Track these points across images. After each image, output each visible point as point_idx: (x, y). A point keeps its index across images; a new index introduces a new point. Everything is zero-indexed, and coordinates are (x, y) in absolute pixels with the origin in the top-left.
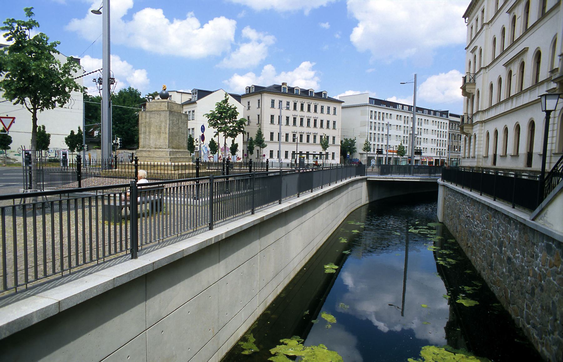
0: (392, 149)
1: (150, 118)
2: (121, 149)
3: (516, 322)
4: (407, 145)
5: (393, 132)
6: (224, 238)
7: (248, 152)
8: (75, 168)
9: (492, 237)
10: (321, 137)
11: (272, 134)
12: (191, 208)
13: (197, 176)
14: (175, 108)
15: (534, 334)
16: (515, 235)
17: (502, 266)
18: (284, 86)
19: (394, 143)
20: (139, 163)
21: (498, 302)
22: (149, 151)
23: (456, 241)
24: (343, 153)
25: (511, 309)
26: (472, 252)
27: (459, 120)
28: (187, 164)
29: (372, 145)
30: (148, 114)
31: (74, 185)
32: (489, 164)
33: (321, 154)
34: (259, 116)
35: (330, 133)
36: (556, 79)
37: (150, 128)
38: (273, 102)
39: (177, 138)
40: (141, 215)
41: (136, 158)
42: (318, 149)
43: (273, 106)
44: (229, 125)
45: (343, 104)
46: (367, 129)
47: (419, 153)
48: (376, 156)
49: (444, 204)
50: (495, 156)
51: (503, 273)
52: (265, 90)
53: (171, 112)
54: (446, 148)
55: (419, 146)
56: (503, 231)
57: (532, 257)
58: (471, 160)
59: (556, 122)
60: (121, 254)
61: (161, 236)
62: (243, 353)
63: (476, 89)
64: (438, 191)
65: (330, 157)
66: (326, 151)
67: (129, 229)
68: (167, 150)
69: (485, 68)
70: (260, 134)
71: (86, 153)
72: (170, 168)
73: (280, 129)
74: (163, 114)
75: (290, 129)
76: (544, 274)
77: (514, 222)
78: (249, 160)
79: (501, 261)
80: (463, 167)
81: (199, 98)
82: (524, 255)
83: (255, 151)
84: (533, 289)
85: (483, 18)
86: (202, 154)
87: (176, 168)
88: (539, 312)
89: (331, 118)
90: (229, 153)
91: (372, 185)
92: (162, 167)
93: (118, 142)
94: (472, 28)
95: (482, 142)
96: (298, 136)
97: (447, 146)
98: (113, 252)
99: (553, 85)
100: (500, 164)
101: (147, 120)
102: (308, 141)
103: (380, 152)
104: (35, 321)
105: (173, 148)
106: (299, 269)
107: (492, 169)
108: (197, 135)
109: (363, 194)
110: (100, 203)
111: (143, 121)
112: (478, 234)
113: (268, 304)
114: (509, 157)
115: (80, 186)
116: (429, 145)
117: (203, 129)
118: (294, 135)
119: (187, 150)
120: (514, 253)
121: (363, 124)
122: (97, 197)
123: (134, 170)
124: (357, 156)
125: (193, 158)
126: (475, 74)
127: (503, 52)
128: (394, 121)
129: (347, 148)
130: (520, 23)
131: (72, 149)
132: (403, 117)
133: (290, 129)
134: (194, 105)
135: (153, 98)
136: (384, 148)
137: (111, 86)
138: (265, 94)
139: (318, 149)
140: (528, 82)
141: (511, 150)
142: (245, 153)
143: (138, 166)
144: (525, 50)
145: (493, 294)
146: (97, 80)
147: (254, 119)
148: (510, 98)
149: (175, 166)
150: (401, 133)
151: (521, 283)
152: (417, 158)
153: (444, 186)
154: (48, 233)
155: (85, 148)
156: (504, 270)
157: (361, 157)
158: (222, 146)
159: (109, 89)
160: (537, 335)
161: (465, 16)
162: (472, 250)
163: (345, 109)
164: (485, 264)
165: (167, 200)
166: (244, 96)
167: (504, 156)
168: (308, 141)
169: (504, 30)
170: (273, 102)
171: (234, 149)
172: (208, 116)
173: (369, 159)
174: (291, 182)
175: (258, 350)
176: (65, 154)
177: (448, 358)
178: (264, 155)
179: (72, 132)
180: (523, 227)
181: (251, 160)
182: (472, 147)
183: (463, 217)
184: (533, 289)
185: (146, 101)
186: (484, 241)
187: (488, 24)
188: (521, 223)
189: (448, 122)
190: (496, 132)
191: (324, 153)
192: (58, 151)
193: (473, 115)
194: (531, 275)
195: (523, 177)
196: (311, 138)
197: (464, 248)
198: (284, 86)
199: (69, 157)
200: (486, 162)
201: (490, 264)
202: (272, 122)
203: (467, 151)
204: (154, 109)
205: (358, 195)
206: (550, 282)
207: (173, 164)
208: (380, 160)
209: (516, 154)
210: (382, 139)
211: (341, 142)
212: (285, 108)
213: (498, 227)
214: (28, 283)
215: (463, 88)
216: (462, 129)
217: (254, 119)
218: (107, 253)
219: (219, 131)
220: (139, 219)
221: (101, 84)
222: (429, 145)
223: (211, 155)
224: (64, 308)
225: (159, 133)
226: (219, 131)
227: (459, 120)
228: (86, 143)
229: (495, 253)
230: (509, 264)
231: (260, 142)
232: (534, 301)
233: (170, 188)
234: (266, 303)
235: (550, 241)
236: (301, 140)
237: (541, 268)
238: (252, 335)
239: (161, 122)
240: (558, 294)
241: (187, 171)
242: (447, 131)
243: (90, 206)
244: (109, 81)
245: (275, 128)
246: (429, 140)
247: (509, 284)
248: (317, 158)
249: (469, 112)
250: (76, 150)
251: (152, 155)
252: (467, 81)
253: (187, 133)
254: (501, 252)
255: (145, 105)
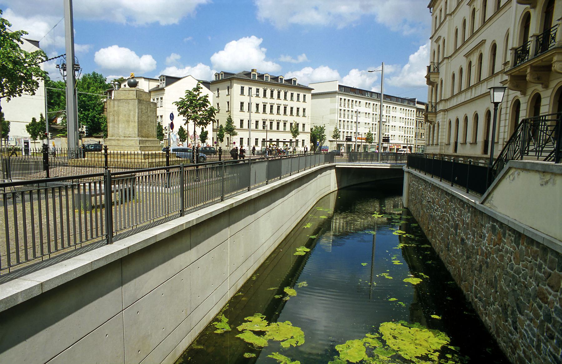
0: (360, 136)
1: (119, 106)
2: (87, 137)
3: (467, 297)
4: (376, 133)
5: (362, 119)
6: (195, 224)
7: (217, 140)
8: (41, 158)
9: (449, 220)
10: (291, 124)
11: (242, 121)
12: (162, 196)
13: (168, 165)
14: (144, 97)
15: (480, 304)
16: (467, 218)
17: (457, 247)
18: (254, 73)
19: (363, 131)
20: (108, 151)
21: (453, 280)
22: (118, 140)
23: (419, 225)
24: (313, 139)
25: (463, 286)
26: (432, 236)
27: (423, 107)
28: (157, 152)
29: (342, 132)
30: (116, 103)
31: (42, 175)
32: (450, 151)
33: (291, 141)
34: (228, 103)
35: (300, 120)
36: (507, 72)
37: (119, 117)
38: (242, 88)
39: (146, 127)
40: (115, 203)
41: (106, 147)
42: (289, 137)
43: (242, 93)
44: (199, 113)
45: (313, 92)
46: (336, 117)
47: (386, 140)
48: (345, 143)
49: (409, 190)
50: (456, 143)
51: (457, 253)
52: (235, 76)
53: (140, 101)
54: (414, 136)
55: (387, 134)
56: (458, 215)
57: (481, 237)
58: (434, 147)
59: (508, 112)
60: (96, 240)
61: (131, 223)
62: (216, 332)
63: (440, 79)
64: (403, 178)
65: (300, 144)
66: (297, 138)
67: (104, 216)
68: (136, 138)
69: (448, 58)
70: (230, 121)
71: (50, 141)
72: (140, 157)
73: (250, 116)
74: (131, 102)
75: (260, 117)
76: (489, 252)
77: (467, 206)
78: (218, 148)
79: (456, 242)
80: (428, 154)
81: (167, 85)
82: (474, 236)
83: (225, 139)
84: (481, 266)
85: (446, 9)
86: (172, 142)
87: (147, 157)
88: (485, 286)
89: (301, 105)
90: (198, 141)
91: (341, 173)
92: (133, 156)
93: (84, 130)
94: (436, 18)
95: (445, 130)
96: (268, 123)
97: (414, 133)
98: (89, 238)
99: (506, 77)
100: (461, 151)
101: (116, 109)
102: (278, 128)
103: (349, 139)
104: (20, 300)
105: (142, 137)
106: (268, 254)
107: (453, 156)
108: (166, 123)
109: (332, 180)
110: (70, 192)
111: (112, 110)
112: (438, 218)
113: (239, 287)
114: (468, 145)
115: (48, 176)
116: (397, 133)
117: (172, 117)
118: (264, 123)
119: (156, 139)
120: (466, 234)
121: (332, 112)
122: (66, 186)
123: (104, 159)
124: (326, 144)
125: (162, 146)
126: (439, 64)
127: (464, 43)
128: (363, 109)
129: (317, 136)
130: (478, 15)
131: (34, 136)
132: (371, 105)
133: (260, 117)
134: (161, 92)
135: (120, 86)
136: (353, 135)
137: (76, 73)
138: (234, 81)
139: (289, 137)
140: (485, 74)
141: (470, 139)
142: (215, 140)
143: (107, 155)
144: (483, 42)
145: (448, 273)
146: (61, 66)
147: (224, 107)
148: (469, 88)
149: (145, 155)
150: (370, 120)
151: (471, 262)
152: (385, 145)
153: (408, 172)
154: (20, 222)
155: (49, 136)
156: (458, 251)
157: (331, 145)
158: (191, 133)
159: (74, 76)
160: (482, 307)
161: (429, 7)
162: (432, 233)
163: (315, 96)
164: (442, 246)
165: (139, 188)
166: (213, 83)
167: (465, 143)
168: (278, 128)
169: (465, 21)
170: (242, 88)
171: (204, 137)
172: (177, 103)
173: (339, 146)
174: (260, 170)
175: (230, 330)
176: (27, 143)
177: (404, 332)
178: (234, 143)
179: (34, 120)
180: (475, 211)
181: (220, 148)
182: (435, 135)
183: (424, 203)
184: (481, 266)
185: (112, 87)
186: (442, 224)
187: (451, 15)
188: (472, 207)
189: (415, 110)
190: (466, 119)
191: (294, 140)
192: (19, 140)
193: (436, 104)
194: (479, 253)
195: (480, 165)
196: (281, 125)
197: (425, 231)
198: (254, 73)
199: (31, 146)
200: (448, 149)
201: (447, 246)
202: (242, 109)
203: (431, 139)
204: (122, 98)
205: (329, 182)
206: (493, 258)
207: (143, 152)
208: (349, 147)
209: (474, 142)
210: (352, 127)
211: (311, 129)
212: (255, 96)
213: (454, 211)
214: (11, 267)
215: (428, 77)
216: (426, 117)
217: (224, 107)
218: (84, 240)
219: (188, 119)
220: (113, 207)
221: (64, 70)
222: (397, 133)
223: (181, 143)
224: (47, 289)
225: (128, 122)
226: (188, 119)
227: (423, 107)
228: (49, 131)
229: (451, 235)
230: (462, 245)
231: (231, 130)
232: (481, 277)
233: (142, 177)
234: (236, 287)
235: (494, 222)
236: (271, 127)
237: (487, 247)
238: (223, 315)
239: (130, 110)
240: (499, 269)
241: (157, 160)
242: (414, 118)
243: (60, 196)
244: (73, 67)
245: (245, 116)
246: (397, 127)
247: (462, 263)
248: (287, 145)
249: (433, 101)
250: (38, 137)
251: (122, 143)
252: (432, 70)
253: (156, 121)
254: (456, 234)
255: (110, 92)
